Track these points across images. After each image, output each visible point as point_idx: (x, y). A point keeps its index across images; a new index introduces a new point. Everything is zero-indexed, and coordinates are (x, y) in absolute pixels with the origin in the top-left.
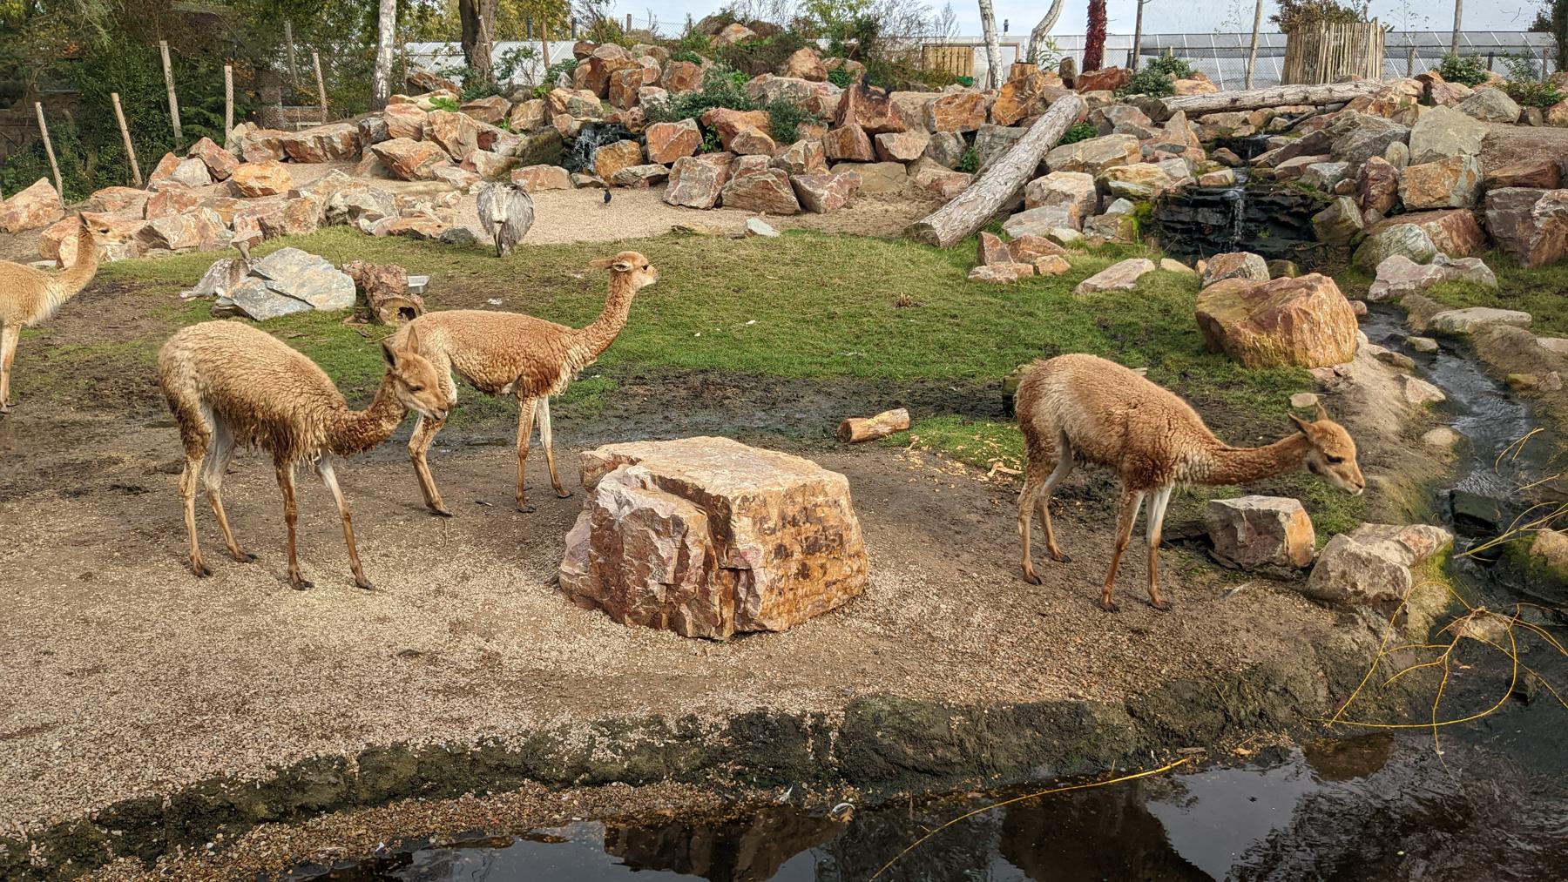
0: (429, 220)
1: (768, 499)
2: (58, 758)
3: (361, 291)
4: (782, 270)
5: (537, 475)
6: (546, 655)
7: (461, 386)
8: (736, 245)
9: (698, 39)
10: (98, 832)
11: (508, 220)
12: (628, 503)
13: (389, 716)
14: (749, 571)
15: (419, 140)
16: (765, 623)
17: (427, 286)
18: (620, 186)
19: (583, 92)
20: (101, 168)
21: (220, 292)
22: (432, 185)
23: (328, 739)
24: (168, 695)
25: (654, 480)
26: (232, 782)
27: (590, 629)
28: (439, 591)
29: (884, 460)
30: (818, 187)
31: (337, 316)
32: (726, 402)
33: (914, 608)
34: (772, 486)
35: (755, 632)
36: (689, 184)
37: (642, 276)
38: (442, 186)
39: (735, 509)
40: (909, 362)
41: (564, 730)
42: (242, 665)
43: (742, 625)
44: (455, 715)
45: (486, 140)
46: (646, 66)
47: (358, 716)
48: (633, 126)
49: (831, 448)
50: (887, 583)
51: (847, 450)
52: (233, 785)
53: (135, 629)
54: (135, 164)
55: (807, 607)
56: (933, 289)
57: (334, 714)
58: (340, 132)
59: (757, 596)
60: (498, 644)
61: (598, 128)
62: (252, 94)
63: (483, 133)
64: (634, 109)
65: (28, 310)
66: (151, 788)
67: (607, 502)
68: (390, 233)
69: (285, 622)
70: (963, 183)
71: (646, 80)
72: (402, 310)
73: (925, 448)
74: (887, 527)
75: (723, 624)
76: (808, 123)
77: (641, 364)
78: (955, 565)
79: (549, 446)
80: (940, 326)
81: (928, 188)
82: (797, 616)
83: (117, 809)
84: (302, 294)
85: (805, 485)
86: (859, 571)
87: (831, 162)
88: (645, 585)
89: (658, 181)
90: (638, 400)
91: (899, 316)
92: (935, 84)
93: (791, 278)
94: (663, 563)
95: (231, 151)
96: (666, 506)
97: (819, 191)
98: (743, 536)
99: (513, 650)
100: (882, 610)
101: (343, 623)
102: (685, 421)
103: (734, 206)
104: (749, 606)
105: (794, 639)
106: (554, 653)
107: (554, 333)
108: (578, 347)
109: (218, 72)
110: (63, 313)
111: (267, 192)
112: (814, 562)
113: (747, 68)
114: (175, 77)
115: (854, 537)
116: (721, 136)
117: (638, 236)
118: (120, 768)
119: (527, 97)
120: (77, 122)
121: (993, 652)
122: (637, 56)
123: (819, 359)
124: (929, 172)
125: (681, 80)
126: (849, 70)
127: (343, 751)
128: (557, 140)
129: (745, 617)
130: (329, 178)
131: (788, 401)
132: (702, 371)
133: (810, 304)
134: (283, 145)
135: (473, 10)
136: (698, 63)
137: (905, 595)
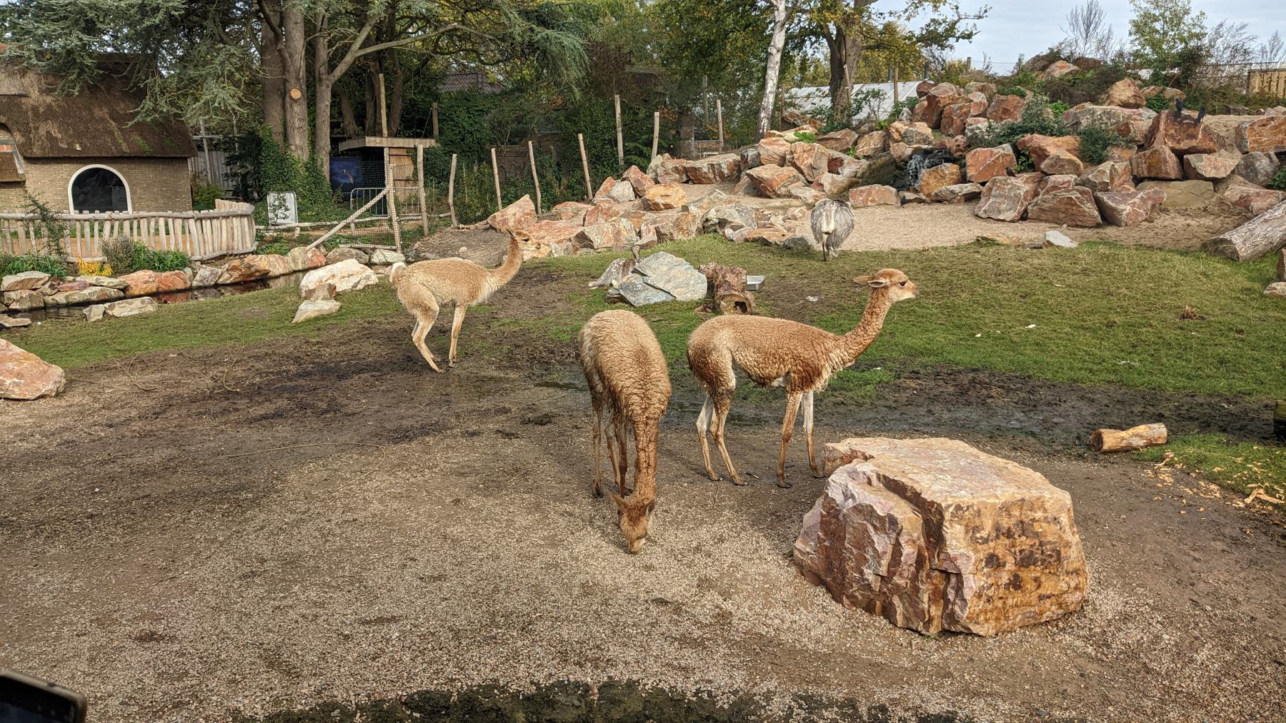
0: (776, 231)
1: (983, 510)
2: (393, 646)
3: (712, 287)
4: (1071, 279)
5: (794, 454)
6: (770, 622)
7: (739, 378)
8: (1032, 254)
9: (1026, 75)
10: (404, 712)
11: (835, 230)
12: (853, 496)
13: (631, 654)
14: (959, 575)
15: (782, 166)
16: (971, 626)
17: (763, 284)
18: (940, 202)
19: (918, 124)
20: (569, 187)
21: (614, 283)
22: (787, 201)
23: (581, 666)
24: (480, 607)
25: (878, 476)
26: (503, 690)
27: (813, 604)
28: (698, 549)
29: (1132, 474)
30: (1120, 202)
31: (691, 305)
32: (989, 401)
33: (1134, 634)
34: (988, 497)
35: (961, 633)
36: (999, 200)
37: (899, 292)
38: (795, 202)
39: (947, 516)
40: (1182, 375)
41: (768, 696)
42: (538, 591)
43: (949, 624)
44: (683, 663)
45: (834, 165)
46: (975, 100)
47: (608, 650)
48: (957, 151)
49: (1080, 457)
50: (1109, 603)
51: (1096, 460)
52: (503, 692)
53: (475, 548)
54: (589, 185)
55: (1017, 617)
56: (1223, 301)
57: (591, 644)
58: (726, 160)
59: (965, 600)
60: (733, 604)
61: (926, 153)
62: (674, 132)
63: (833, 159)
64: (959, 137)
65: (473, 296)
66: (446, 684)
67: (835, 493)
68: (746, 240)
69: (577, 559)
70: (1273, 200)
71: (973, 112)
72: (737, 303)
73: (1179, 466)
74: (1119, 544)
75: (931, 620)
76: (1117, 146)
77: (919, 360)
78: (1188, 593)
79: (810, 432)
80: (1223, 340)
81: (1235, 204)
82: (1006, 625)
83: (419, 696)
84: (668, 287)
85: (1023, 500)
86: (1076, 588)
87: (1138, 180)
88: (862, 573)
89: (972, 198)
90: (908, 394)
91: (1182, 328)
92: (1255, 106)
93: (1078, 287)
94: (878, 556)
95: (650, 175)
96: (885, 504)
97: (1121, 207)
98: (954, 542)
99: (743, 611)
100: (1098, 630)
101: (618, 566)
102: (946, 415)
103: (1038, 219)
104: (956, 608)
105: (1000, 647)
106: (777, 621)
107: (819, 338)
108: (838, 351)
109: (650, 117)
110: (502, 294)
111: (668, 207)
112: (1028, 575)
113: (1067, 98)
114: (623, 120)
115: (1074, 554)
116: (1034, 158)
117: (945, 245)
118: (430, 663)
119: (872, 130)
120: (558, 154)
121: (1213, 695)
122: (968, 92)
123: (1090, 365)
124: (1235, 190)
125: (1006, 111)
126: (1167, 97)
127: (589, 679)
128: (892, 164)
129: (951, 617)
130: (711, 197)
131: (1049, 404)
132: (974, 370)
133: (1092, 312)
134: (686, 170)
135: (840, 60)
136: (1023, 96)
137: (1126, 618)
